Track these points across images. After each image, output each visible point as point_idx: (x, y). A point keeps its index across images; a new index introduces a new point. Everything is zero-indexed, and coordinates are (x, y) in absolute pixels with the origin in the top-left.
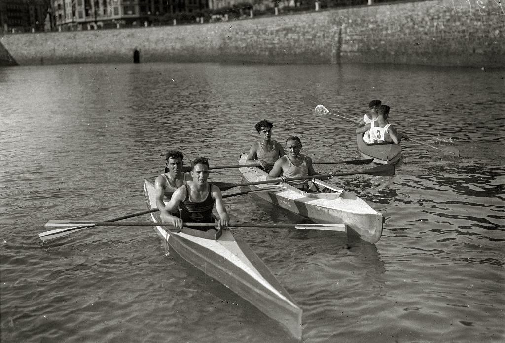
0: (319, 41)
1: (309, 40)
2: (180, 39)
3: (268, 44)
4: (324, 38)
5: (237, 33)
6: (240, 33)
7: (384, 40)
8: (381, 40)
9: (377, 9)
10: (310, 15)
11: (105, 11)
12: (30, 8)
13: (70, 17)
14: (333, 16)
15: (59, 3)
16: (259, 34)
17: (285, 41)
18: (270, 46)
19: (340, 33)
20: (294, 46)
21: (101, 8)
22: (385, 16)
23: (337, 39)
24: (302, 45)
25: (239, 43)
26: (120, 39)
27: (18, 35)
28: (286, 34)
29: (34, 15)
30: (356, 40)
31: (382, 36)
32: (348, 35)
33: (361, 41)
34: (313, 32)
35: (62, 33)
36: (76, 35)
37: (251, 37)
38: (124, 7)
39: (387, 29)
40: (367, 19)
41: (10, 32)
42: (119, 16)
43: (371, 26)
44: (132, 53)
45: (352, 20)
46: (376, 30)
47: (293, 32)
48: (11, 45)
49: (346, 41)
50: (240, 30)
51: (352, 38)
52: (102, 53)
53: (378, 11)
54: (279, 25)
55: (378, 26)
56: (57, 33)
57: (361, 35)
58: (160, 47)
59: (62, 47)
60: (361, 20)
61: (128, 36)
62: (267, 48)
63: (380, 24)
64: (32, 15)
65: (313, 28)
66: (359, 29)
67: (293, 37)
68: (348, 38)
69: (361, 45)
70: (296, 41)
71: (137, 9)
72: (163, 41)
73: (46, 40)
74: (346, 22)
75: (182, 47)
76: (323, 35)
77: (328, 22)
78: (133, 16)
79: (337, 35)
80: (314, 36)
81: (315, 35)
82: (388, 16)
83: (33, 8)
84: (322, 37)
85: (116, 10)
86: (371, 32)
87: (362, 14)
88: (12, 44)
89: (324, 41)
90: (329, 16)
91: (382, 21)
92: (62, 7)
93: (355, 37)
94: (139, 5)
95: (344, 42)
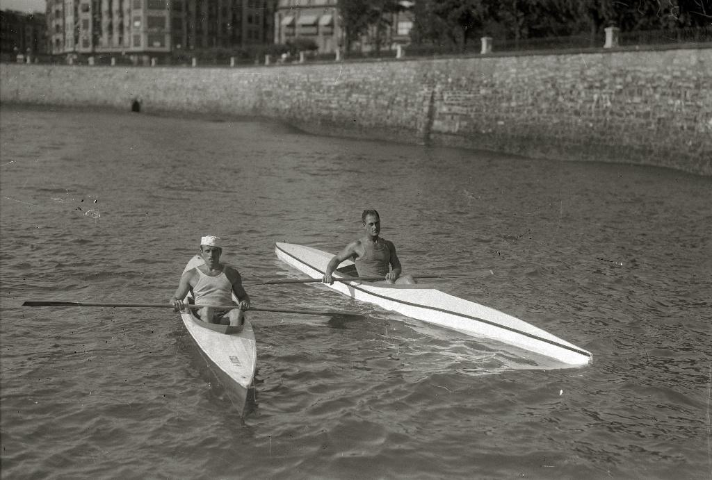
3: (321, 108)
4: (406, 106)
6: (284, 86)
7: (503, 120)
8: (497, 119)
10: (388, 65)
11: (121, 39)
13: (70, 45)
16: (310, 90)
17: (346, 105)
18: (325, 112)
19: (432, 100)
20: (360, 115)
21: (116, 35)
22: (508, 77)
23: (426, 109)
25: (282, 102)
28: (349, 95)
29: (31, 38)
30: (457, 114)
31: (500, 111)
32: (445, 104)
33: (465, 117)
34: (389, 94)
36: (50, 71)
37: (298, 94)
39: (509, 99)
40: (477, 79)
43: (483, 91)
46: (491, 99)
47: (361, 91)
49: (440, 114)
51: (450, 110)
52: (87, 101)
53: (498, 65)
57: (466, 106)
60: (468, 79)
61: (127, 78)
62: (320, 114)
63: (499, 90)
64: (29, 37)
65: (391, 88)
66: (463, 95)
67: (360, 100)
68: (445, 109)
69: (464, 123)
70: (364, 107)
71: (168, 39)
76: (406, 100)
77: (415, 79)
79: (427, 103)
80: (392, 101)
81: (394, 100)
82: (514, 76)
83: (31, 28)
84: (403, 104)
85: (137, 38)
86: (482, 102)
87: (469, 69)
90: (416, 69)
91: (502, 84)
93: (456, 109)
95: (437, 116)
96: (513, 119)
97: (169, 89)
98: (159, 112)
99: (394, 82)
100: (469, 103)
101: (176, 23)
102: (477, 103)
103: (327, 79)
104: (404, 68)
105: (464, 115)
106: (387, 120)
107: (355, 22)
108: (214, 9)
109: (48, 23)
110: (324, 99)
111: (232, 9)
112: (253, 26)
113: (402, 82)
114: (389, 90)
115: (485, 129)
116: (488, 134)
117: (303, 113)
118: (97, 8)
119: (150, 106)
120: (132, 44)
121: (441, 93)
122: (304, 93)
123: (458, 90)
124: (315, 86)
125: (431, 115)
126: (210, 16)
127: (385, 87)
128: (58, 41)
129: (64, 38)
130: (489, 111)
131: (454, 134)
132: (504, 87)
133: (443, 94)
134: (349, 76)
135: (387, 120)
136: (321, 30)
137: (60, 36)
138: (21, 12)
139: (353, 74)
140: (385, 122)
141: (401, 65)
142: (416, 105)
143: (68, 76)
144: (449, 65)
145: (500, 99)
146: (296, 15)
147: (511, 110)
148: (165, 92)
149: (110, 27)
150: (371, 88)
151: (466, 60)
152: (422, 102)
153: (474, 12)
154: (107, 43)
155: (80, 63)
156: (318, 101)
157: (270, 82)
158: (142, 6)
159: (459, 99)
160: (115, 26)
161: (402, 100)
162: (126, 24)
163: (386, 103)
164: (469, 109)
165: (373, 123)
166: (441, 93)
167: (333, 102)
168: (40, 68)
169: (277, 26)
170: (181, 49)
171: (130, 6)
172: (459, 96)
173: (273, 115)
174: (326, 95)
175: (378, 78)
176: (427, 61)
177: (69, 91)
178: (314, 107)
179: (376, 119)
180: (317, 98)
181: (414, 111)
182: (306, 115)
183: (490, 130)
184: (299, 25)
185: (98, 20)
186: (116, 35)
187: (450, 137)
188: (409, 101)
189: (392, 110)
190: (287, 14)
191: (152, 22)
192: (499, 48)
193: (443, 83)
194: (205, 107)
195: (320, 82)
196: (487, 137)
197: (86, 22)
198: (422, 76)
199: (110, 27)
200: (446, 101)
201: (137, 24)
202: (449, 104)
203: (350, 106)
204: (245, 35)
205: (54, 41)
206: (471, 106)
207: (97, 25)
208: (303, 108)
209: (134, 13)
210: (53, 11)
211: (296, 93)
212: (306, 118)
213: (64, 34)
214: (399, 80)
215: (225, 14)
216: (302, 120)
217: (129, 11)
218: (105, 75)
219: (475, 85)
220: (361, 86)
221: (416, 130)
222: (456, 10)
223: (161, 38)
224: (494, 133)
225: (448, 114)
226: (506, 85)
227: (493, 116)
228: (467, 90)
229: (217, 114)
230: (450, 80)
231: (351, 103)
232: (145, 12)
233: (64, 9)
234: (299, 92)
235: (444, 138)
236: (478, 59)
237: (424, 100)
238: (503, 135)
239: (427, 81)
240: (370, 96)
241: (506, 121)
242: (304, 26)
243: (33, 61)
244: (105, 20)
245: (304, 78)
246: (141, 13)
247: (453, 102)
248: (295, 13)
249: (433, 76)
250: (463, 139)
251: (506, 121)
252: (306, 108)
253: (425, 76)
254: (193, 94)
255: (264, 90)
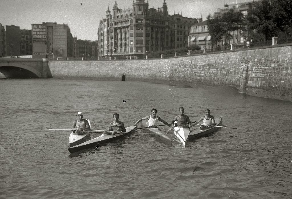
0: (231, 76)
1: (224, 75)
2: (148, 69)
3: (197, 76)
4: (235, 74)
5: (180, 66)
6: (181, 66)
7: (283, 80)
8: (281, 79)
9: (279, 50)
10: (226, 54)
11: (125, 50)
12: (92, 46)
13: (106, 53)
14: (243, 55)
15: (101, 44)
16: (192, 68)
17: (208, 74)
18: (198, 78)
19: (247, 71)
20: (214, 79)
21: (123, 48)
22: (286, 57)
23: (244, 75)
24: (219, 79)
25: (181, 74)
26: (115, 67)
27: (59, 62)
28: (209, 69)
29: (94, 51)
30: (260, 78)
31: (282, 75)
32: (254, 72)
33: (264, 79)
34: (227, 68)
35: (84, 62)
36: (91, 63)
37: (188, 70)
38: (136, 48)
39: (287, 69)
40: (270, 59)
41: (55, 59)
42: (133, 53)
43: (273, 65)
44: (121, 77)
45: (257, 59)
46: (277, 69)
47: (214, 67)
48: (55, 68)
49: (251, 77)
50: (181, 64)
51: (256, 75)
52: (105, 75)
53: (280, 51)
54: (205, 61)
55: (280, 65)
56: (81, 62)
57: (264, 73)
58: (137, 74)
59: (83, 70)
60: (265, 59)
61: (120, 65)
62: (196, 79)
63: (282, 64)
64: (93, 51)
65: (228, 65)
66: (263, 67)
67: (214, 72)
68: (253, 75)
69: (263, 82)
70: (215, 75)
71: (144, 49)
72: (139, 70)
73: (75, 66)
74: (253, 60)
75: (149, 74)
76: (235, 71)
77: (239, 60)
78: (141, 53)
79: (245, 72)
80: (228, 71)
81: (229, 71)
82: (289, 56)
83: (94, 47)
84: (233, 73)
85: (131, 49)
86: (273, 71)
87: (266, 54)
88: (56, 67)
89: (235, 76)
90: (239, 55)
91: (283, 61)
92: (103, 47)
93: (259, 75)
94: (145, 46)
95: (250, 79)
96: (289, 79)
97: (137, 69)
98: (134, 79)
99: (229, 62)
100: (266, 72)
101: (147, 42)
102: (270, 72)
103: (200, 62)
104: (234, 55)
105: (263, 78)
106: (226, 81)
107: (215, 36)
108: (163, 36)
109: (98, 44)
110: (198, 72)
111: (171, 35)
112: (179, 42)
113: (233, 62)
114: (227, 67)
115: (274, 85)
116: (276, 87)
117: (189, 78)
118: (116, 37)
119: (129, 77)
120: (130, 51)
121: (252, 67)
122: (190, 69)
123: (260, 65)
124: (194, 65)
125: (247, 78)
126: (161, 39)
127: (225, 65)
128: (101, 51)
129: (104, 50)
130: (276, 75)
131: (258, 88)
132: (284, 62)
133: (253, 68)
134: (209, 60)
135: (226, 81)
136: (207, 42)
137: (102, 49)
138: (91, 41)
139: (211, 59)
140: (225, 82)
141: (232, 53)
142: (240, 73)
143: (98, 65)
144: (256, 52)
145: (282, 69)
146: (197, 37)
147: (288, 74)
148: (135, 71)
149: (121, 44)
150: (219, 66)
151: (264, 50)
152: (242, 72)
153: (270, 26)
154: (120, 51)
155: (72, 60)
156: (196, 73)
157: (176, 65)
158: (134, 35)
159: (261, 69)
160: (123, 44)
161: (233, 71)
162: (127, 43)
163: (226, 73)
164: (266, 74)
165: (219, 83)
166: (252, 67)
167: (202, 73)
168: (87, 62)
169: (189, 42)
170: (147, 52)
171: (129, 36)
172: (261, 68)
173: (177, 80)
174: (199, 70)
175: (222, 61)
176: (245, 51)
177: (98, 71)
178: (194, 75)
179: (221, 81)
180: (195, 72)
181: (238, 77)
182: (191, 79)
183: (277, 86)
184: (198, 41)
185: (116, 42)
186: (123, 48)
187: (256, 89)
188: (236, 71)
189: (228, 76)
190: (193, 36)
191: (137, 42)
192: (281, 42)
193: (252, 62)
194: (151, 77)
195: (196, 64)
196: (275, 89)
197: (111, 43)
198: (242, 58)
199: (121, 44)
200: (254, 71)
201: (132, 43)
202: (255, 73)
203: (209, 75)
204: (176, 46)
205: (100, 51)
206: (267, 73)
207: (116, 44)
208: (189, 76)
209: (131, 39)
210: (100, 39)
211: (187, 69)
212: (191, 81)
213: (104, 48)
214: (231, 61)
215: (167, 38)
216: (189, 82)
217: (129, 38)
218: (112, 64)
219: (269, 62)
220: (214, 65)
221: (240, 86)
222: (260, 26)
223: (141, 48)
224: (279, 87)
225: (255, 78)
226: (285, 61)
227: (278, 78)
228: (265, 65)
229: (156, 80)
230: (256, 60)
231: (210, 73)
232: (135, 38)
233: (104, 38)
234: (188, 69)
235: (253, 90)
236: (270, 49)
237: (243, 71)
238: (284, 88)
239: (245, 61)
240: (218, 70)
241: (285, 80)
242: (200, 41)
243: (84, 59)
244: (119, 42)
245: (190, 62)
246: (133, 38)
247: (258, 71)
248: (196, 36)
249: (247, 58)
250: (263, 90)
251: (285, 80)
252: (190, 76)
253: (244, 58)
254: (146, 71)
255: (174, 68)
